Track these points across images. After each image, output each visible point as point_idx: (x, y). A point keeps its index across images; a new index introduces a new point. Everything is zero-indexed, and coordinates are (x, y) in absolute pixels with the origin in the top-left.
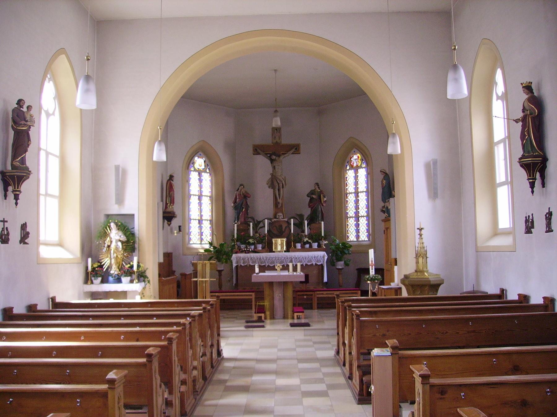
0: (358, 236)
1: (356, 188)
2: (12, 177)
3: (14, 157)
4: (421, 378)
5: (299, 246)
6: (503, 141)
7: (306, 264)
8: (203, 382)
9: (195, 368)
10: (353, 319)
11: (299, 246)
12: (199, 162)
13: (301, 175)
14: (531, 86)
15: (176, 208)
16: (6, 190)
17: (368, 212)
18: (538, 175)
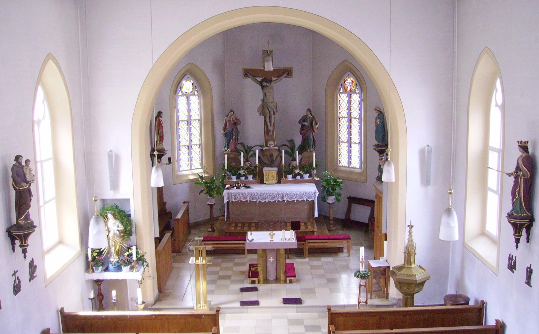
0: (350, 163)
1: (349, 114)
3: (18, 216)
5: (290, 177)
7: (297, 200)
11: (290, 177)
12: (187, 85)
13: (292, 98)
15: (166, 145)
16: (13, 244)
17: (360, 114)
18: (524, 230)
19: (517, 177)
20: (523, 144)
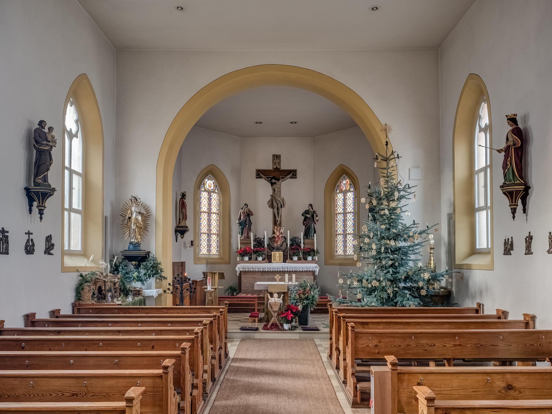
0: (345, 251)
2: (37, 193)
3: (36, 175)
4: (426, 401)
6: (484, 169)
8: (211, 383)
9: (205, 371)
10: (347, 329)
12: (209, 183)
14: (515, 119)
15: (189, 223)
16: (31, 206)
18: (520, 202)
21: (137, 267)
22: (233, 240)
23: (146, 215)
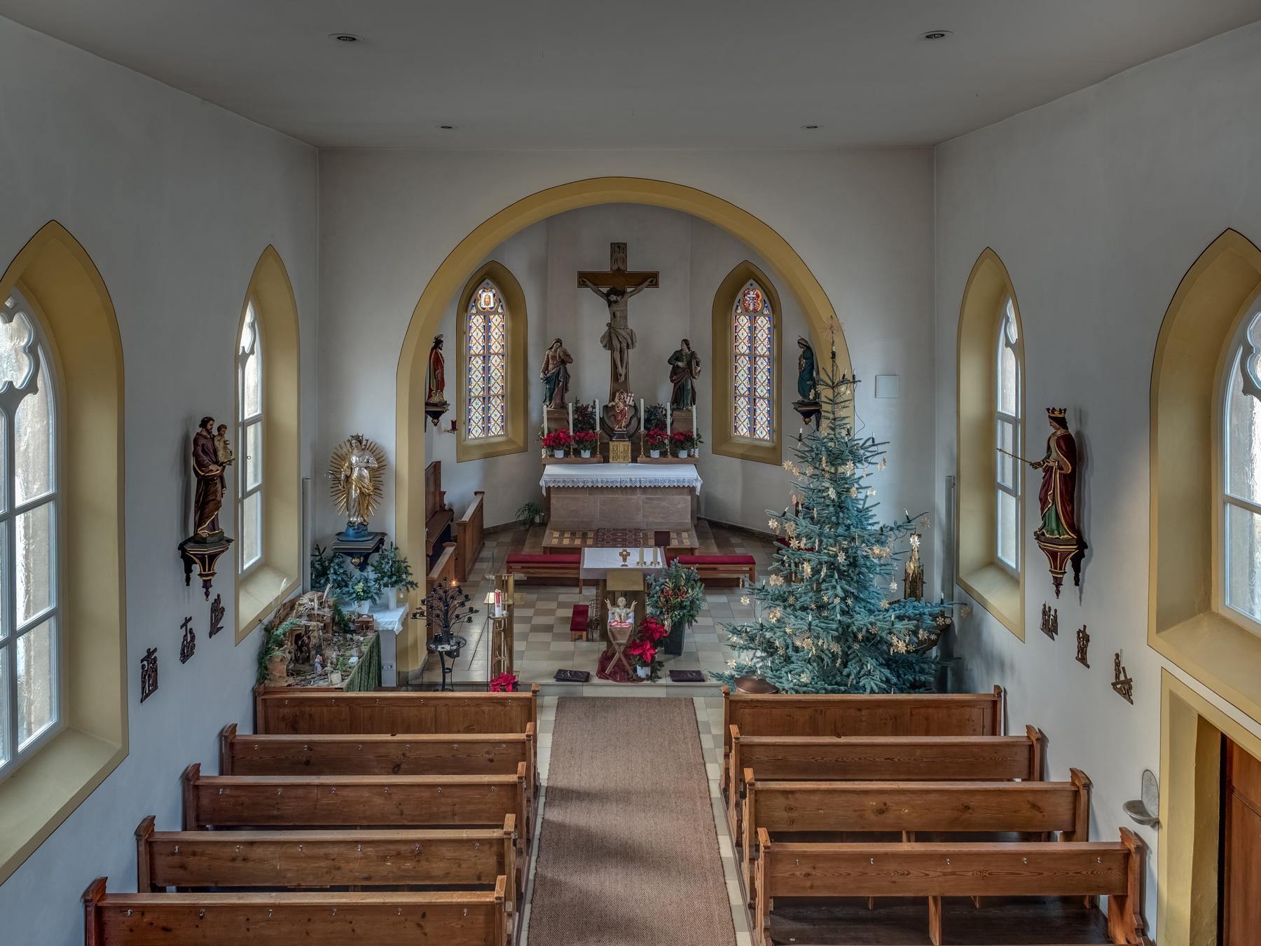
0: (753, 430)
1: (752, 348)
12: (487, 298)
16: (188, 570)
18: (1069, 566)
19: (1048, 470)
20: (1057, 414)
21: (362, 567)
22: (534, 416)
23: (379, 469)
